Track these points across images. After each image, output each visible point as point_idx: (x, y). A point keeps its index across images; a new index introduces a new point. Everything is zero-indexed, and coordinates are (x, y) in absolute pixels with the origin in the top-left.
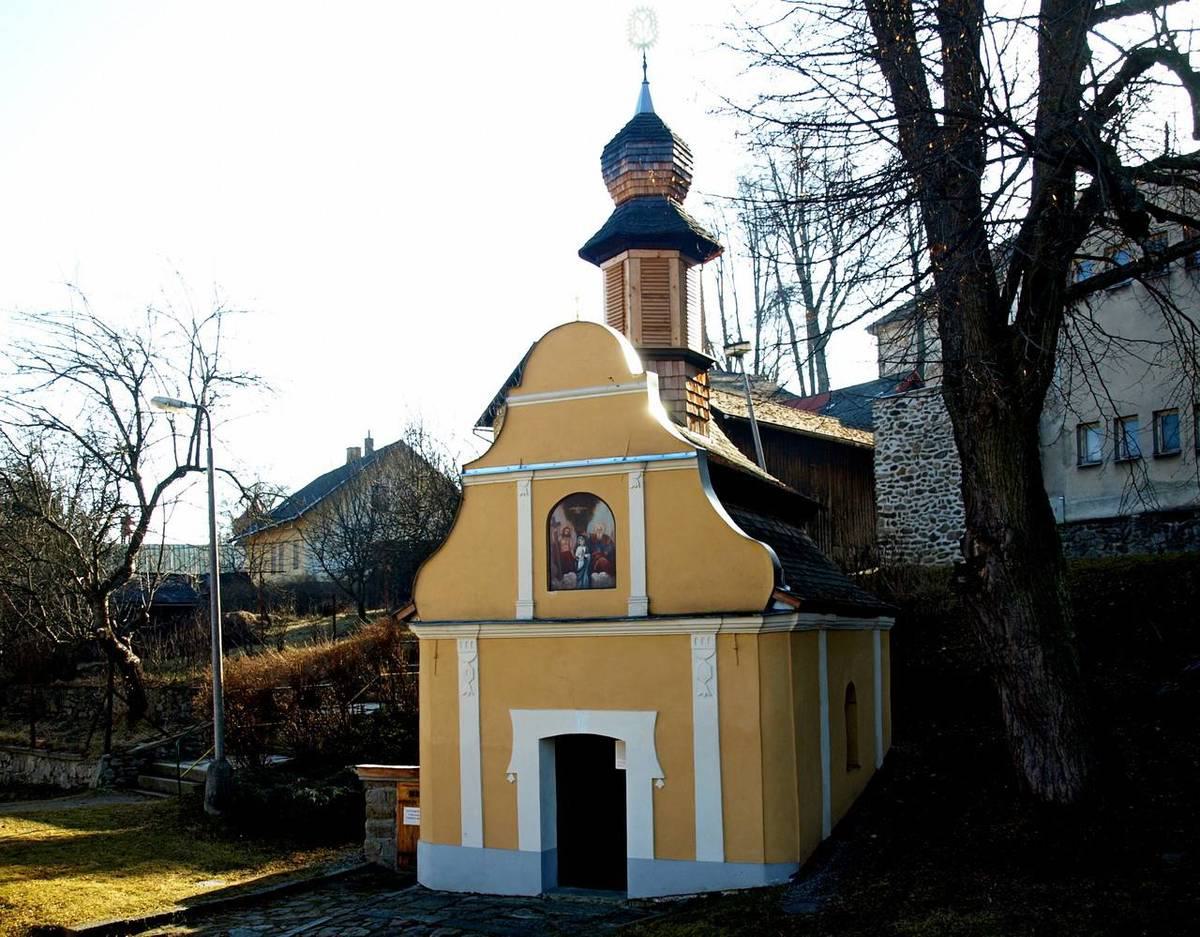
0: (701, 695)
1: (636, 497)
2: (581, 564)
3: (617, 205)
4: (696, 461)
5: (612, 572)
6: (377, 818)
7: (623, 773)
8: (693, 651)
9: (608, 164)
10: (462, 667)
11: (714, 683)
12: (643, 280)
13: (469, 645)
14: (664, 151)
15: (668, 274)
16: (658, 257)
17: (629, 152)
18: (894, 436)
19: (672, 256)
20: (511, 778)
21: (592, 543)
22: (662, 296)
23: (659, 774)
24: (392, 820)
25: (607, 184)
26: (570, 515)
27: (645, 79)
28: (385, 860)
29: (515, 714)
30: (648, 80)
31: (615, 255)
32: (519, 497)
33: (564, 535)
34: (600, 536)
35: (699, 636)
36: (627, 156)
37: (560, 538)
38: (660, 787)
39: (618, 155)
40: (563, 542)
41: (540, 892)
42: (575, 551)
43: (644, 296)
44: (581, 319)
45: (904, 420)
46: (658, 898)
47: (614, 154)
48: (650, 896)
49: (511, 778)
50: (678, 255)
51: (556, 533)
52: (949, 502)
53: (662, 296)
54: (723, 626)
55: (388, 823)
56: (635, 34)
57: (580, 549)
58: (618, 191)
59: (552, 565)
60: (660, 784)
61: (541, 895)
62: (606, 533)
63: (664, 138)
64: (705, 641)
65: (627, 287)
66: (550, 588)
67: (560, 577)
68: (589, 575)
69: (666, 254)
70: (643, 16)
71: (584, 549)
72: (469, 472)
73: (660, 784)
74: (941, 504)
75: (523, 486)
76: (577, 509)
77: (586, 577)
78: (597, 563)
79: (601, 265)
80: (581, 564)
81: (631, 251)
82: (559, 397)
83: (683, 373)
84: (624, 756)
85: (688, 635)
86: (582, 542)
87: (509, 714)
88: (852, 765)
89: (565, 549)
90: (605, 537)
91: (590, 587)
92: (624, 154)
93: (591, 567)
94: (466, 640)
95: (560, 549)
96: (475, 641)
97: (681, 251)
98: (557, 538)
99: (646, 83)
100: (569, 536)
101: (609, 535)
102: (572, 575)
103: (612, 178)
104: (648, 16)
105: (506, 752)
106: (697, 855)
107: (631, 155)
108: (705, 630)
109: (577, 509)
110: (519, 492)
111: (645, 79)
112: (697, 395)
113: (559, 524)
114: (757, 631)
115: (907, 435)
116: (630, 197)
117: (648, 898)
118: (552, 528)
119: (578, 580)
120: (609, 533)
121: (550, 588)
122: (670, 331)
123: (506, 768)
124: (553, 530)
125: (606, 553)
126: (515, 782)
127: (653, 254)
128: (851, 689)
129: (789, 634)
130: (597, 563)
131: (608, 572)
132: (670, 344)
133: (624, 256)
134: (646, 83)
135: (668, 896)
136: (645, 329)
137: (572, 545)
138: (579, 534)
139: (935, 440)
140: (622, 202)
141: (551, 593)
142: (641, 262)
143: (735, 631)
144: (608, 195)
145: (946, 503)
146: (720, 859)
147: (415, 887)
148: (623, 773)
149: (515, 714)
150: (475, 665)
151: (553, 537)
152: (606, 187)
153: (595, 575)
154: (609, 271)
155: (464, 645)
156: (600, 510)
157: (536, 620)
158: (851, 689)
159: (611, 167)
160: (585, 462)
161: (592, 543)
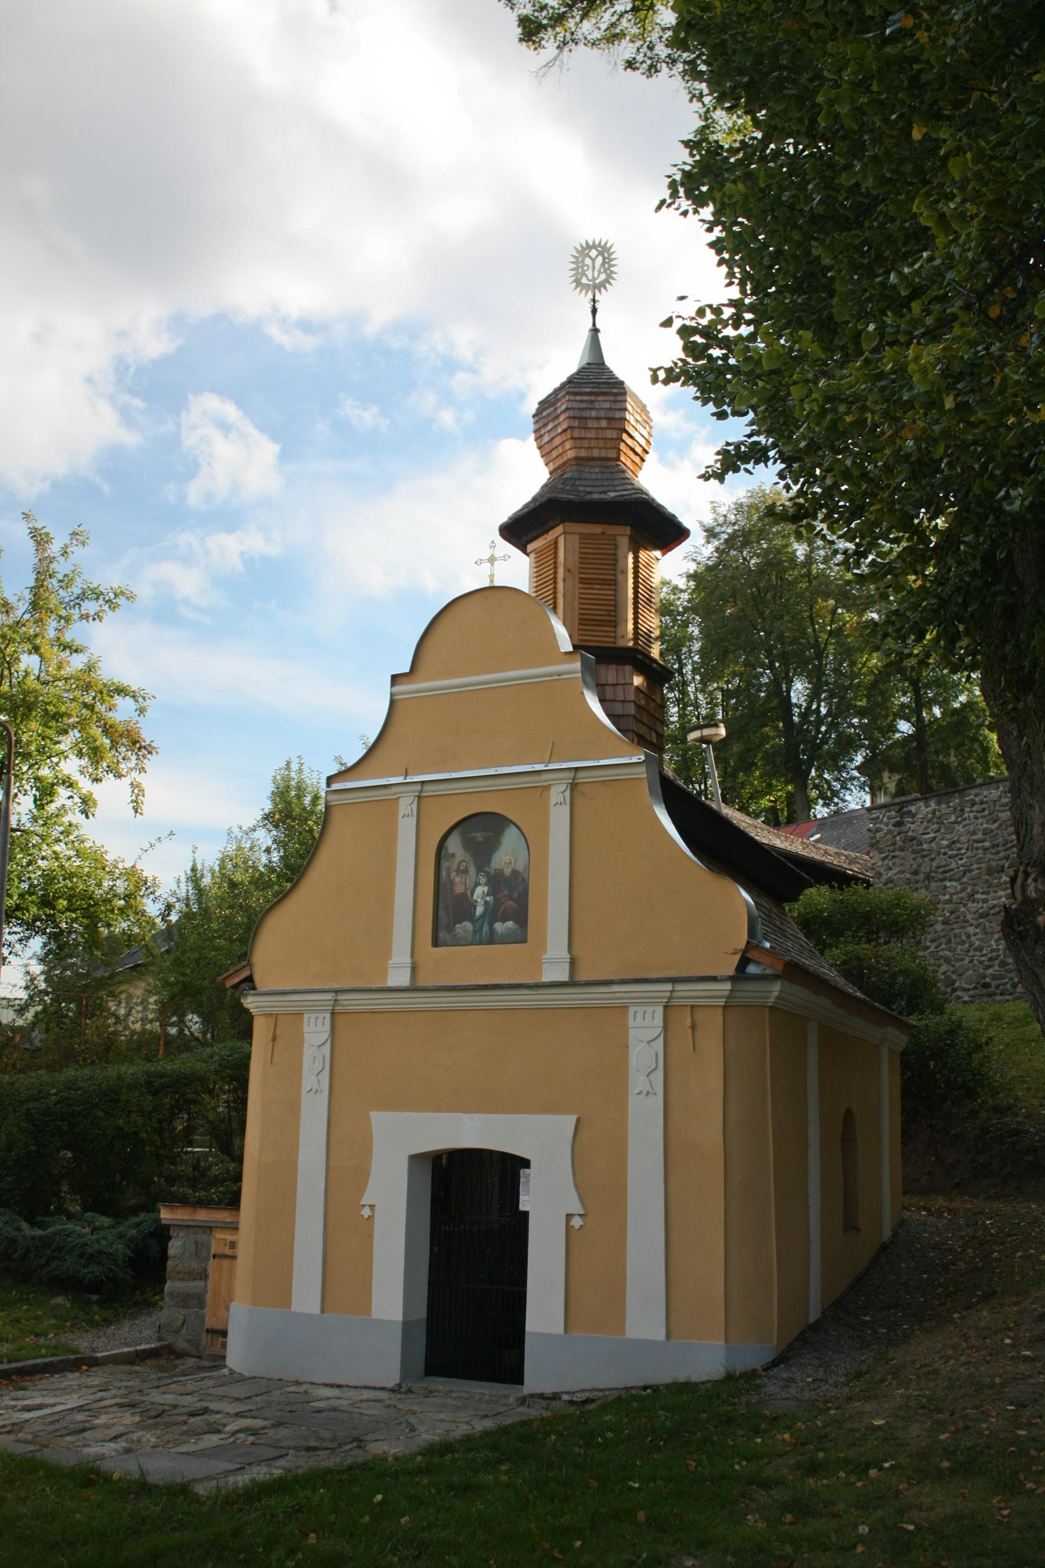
0: (640, 1093)
1: (559, 818)
2: (480, 910)
3: (551, 473)
4: (643, 769)
5: (522, 919)
6: (182, 1280)
7: (526, 1214)
8: (631, 1031)
9: (541, 424)
10: (308, 1053)
11: (659, 1077)
12: (584, 559)
13: (320, 1021)
14: (618, 406)
15: (615, 555)
16: (603, 534)
17: (570, 405)
18: (897, 853)
19: (622, 535)
20: (366, 1212)
21: (496, 882)
22: (605, 582)
23: (577, 1208)
24: (202, 1283)
25: (540, 448)
26: (468, 844)
27: (594, 324)
28: (188, 1341)
29: (375, 1116)
30: (598, 326)
31: (547, 532)
32: (400, 819)
33: (459, 871)
34: (508, 871)
35: (641, 1010)
36: (567, 409)
37: (453, 875)
38: (577, 1227)
39: (556, 409)
40: (457, 880)
41: (397, 1381)
42: (473, 893)
43: (582, 581)
44: (496, 584)
45: (910, 833)
46: (565, 1393)
47: (551, 409)
48: (555, 1390)
49: (366, 1212)
50: (629, 533)
51: (448, 868)
52: (968, 936)
53: (605, 582)
54: (675, 994)
55: (196, 1286)
56: (584, 274)
57: (480, 890)
58: (554, 454)
59: (442, 913)
60: (577, 1222)
61: (400, 1385)
62: (517, 868)
63: (614, 391)
64: (648, 1016)
65: (561, 571)
66: (436, 943)
67: (450, 929)
68: (491, 925)
69: (612, 530)
70: (593, 253)
71: (486, 889)
72: (335, 786)
73: (577, 1222)
74: (958, 940)
75: (407, 805)
76: (479, 835)
77: (486, 928)
78: (502, 909)
79: (530, 547)
80: (480, 910)
81: (567, 524)
82: (460, 687)
83: (633, 698)
84: (528, 1193)
85: (625, 1008)
86: (483, 880)
87: (368, 1119)
88: (850, 1226)
89: (459, 889)
90: (515, 873)
91: (491, 942)
92: (564, 407)
93: (494, 914)
94: (315, 1015)
95: (452, 889)
96: (328, 1016)
97: (633, 528)
98: (449, 874)
99: (595, 331)
100: (466, 872)
101: (521, 869)
102: (468, 925)
103: (546, 438)
104: (600, 253)
105: (361, 1174)
106: (627, 1331)
107: (573, 409)
108: (648, 1001)
109: (479, 836)
110: (401, 813)
111: (594, 324)
112: (649, 712)
113: (453, 855)
114: (722, 1002)
115: (913, 852)
116: (568, 460)
117: (554, 1393)
118: (443, 861)
119: (475, 932)
120: (520, 867)
121: (436, 943)
122: (615, 626)
123: (361, 1198)
124: (445, 864)
125: (515, 895)
126: (371, 1218)
127: (596, 529)
128: (849, 1114)
129: (767, 1010)
130: (502, 909)
131: (517, 922)
132: (615, 643)
133: (560, 529)
134: (595, 331)
135: (582, 1391)
136: (582, 622)
137: (470, 883)
138: (479, 870)
139: (950, 857)
140: (558, 468)
141: (440, 950)
142: (581, 539)
143: (692, 1002)
144: (541, 462)
145: (964, 938)
146: (660, 1335)
147: (225, 1371)
148: (526, 1214)
149: (375, 1116)
150: (327, 1050)
151: (444, 874)
152: (538, 451)
153: (499, 926)
154: (539, 552)
155: (312, 1023)
156: (510, 838)
157: (412, 989)
158: (849, 1114)
159: (545, 425)
160: (492, 771)
161: (496, 882)
